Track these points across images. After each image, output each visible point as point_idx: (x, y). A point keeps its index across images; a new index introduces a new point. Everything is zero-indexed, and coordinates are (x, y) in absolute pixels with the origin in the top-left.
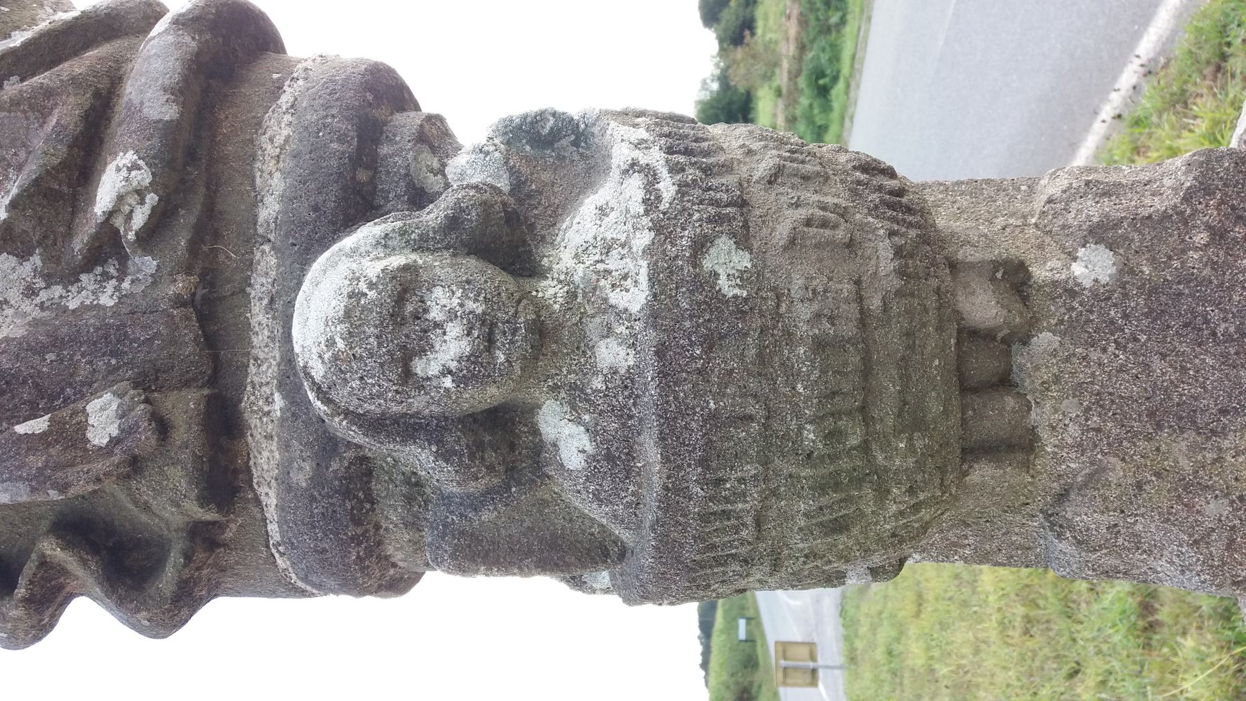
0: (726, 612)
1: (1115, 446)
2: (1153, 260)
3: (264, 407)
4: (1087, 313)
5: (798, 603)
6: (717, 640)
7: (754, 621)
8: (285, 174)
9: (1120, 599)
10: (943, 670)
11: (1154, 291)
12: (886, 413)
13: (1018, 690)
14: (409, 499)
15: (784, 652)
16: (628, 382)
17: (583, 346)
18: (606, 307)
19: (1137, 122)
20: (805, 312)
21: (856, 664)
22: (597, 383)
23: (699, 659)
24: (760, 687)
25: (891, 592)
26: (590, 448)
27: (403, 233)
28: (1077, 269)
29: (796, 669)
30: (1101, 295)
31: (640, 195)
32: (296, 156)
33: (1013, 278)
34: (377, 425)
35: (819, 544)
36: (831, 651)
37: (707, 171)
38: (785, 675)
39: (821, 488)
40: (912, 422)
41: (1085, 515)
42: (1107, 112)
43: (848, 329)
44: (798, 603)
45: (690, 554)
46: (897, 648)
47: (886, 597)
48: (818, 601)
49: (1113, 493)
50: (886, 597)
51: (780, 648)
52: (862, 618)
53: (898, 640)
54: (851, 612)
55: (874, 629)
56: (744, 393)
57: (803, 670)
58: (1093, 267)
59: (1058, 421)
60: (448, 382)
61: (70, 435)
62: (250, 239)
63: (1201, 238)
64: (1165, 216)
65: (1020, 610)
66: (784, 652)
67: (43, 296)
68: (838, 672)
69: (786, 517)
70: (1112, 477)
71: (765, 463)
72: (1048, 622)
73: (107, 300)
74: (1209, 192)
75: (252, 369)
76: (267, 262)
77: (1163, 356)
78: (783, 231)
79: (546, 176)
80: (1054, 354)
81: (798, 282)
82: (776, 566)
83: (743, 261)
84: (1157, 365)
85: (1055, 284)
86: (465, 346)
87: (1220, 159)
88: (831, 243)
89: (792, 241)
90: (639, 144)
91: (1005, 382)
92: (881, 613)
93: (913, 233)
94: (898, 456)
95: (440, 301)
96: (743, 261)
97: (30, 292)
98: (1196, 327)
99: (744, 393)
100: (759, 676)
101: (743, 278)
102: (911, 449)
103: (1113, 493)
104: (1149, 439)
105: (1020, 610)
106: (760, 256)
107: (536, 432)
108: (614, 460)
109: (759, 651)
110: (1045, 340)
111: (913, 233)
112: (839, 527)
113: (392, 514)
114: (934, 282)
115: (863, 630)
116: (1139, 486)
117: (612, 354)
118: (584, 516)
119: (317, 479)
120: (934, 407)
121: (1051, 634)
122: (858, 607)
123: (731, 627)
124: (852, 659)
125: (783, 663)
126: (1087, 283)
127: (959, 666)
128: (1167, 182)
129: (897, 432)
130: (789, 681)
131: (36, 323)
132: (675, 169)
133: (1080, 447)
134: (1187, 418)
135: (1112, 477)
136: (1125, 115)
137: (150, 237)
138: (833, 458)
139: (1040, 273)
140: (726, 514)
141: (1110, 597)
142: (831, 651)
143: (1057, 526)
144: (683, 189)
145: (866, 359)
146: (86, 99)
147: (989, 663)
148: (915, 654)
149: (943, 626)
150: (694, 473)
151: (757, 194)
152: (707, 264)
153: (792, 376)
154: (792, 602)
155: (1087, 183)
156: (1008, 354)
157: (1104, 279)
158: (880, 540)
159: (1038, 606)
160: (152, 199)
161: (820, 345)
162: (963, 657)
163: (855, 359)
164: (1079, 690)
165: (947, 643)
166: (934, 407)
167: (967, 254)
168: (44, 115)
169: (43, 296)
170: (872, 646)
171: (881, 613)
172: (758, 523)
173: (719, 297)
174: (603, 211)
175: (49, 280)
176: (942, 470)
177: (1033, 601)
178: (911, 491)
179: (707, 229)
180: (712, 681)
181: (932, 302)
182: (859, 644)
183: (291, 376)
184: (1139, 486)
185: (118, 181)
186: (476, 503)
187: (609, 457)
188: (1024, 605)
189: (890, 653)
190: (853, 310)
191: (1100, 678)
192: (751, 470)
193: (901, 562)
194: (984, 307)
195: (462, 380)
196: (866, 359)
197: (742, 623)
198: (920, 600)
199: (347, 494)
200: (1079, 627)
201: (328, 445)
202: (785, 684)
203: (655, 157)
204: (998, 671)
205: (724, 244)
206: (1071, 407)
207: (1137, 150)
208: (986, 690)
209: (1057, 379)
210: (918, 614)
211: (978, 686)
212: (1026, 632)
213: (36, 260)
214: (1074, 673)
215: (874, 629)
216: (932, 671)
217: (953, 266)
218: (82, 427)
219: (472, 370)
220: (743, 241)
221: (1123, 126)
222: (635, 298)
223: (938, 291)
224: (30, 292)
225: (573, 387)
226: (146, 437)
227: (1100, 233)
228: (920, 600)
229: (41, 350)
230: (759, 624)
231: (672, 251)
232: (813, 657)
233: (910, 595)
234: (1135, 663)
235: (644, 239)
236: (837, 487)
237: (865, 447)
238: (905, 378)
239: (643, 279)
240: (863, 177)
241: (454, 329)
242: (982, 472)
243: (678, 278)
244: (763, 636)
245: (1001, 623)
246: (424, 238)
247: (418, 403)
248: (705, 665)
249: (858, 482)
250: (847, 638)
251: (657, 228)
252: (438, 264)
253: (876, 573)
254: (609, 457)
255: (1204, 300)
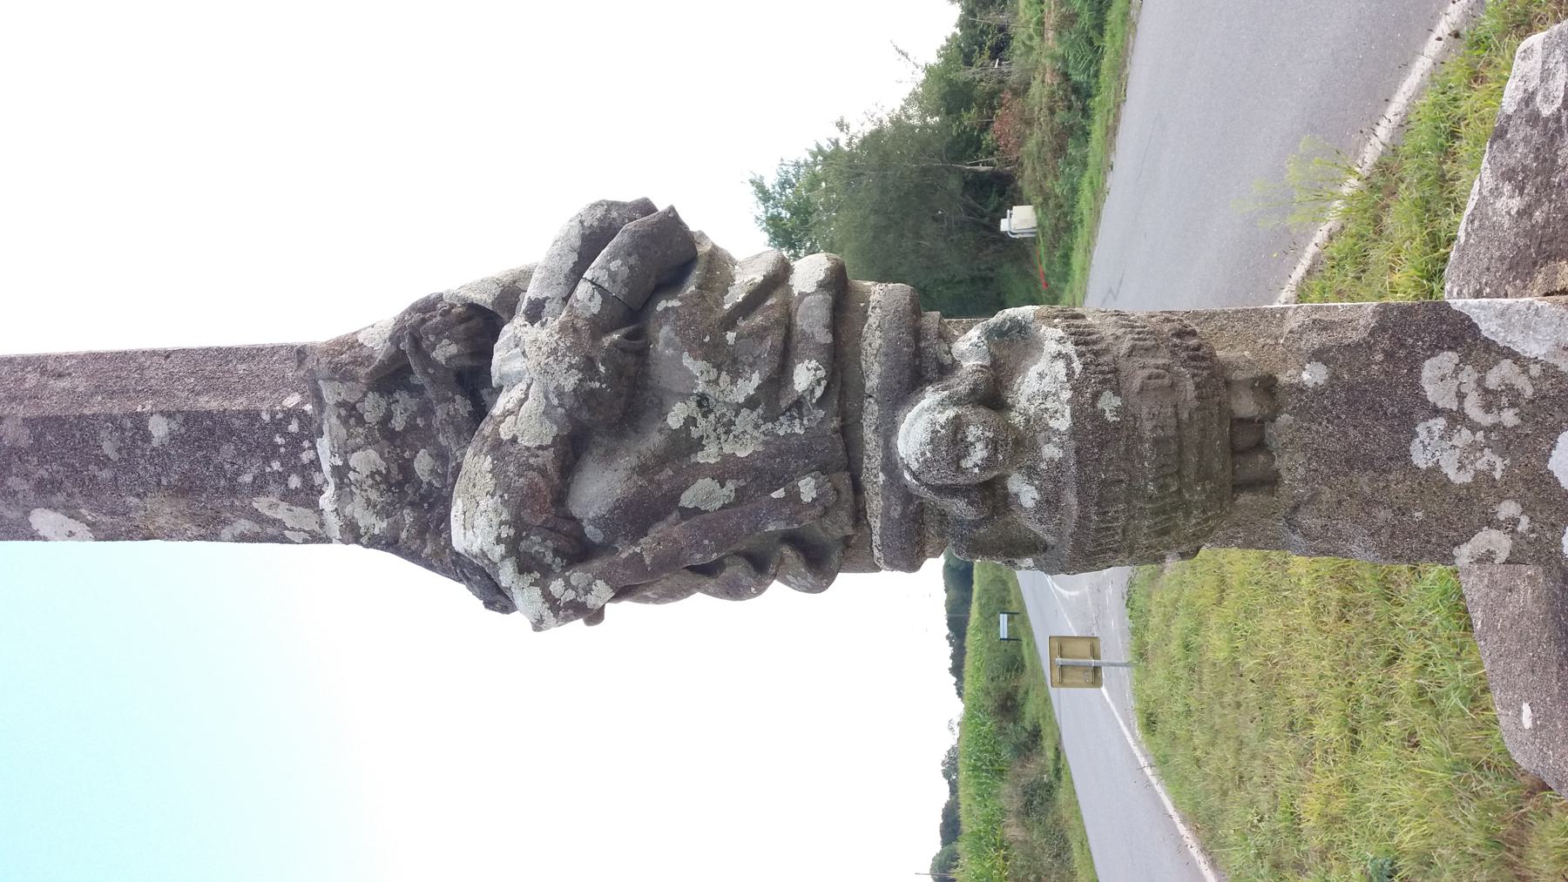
0: (982, 606)
1: (1326, 480)
2: (1350, 371)
3: (875, 479)
4: (1310, 403)
5: (1074, 593)
6: (972, 639)
7: (1018, 616)
8: (881, 364)
9: (1441, 579)
10: (1248, 663)
11: (1351, 389)
12: (1190, 472)
13: (1332, 681)
14: (941, 522)
15: (1061, 648)
16: (1059, 465)
17: (1035, 447)
18: (1047, 428)
19: (1477, 43)
20: (1148, 425)
21: (1146, 660)
22: (1043, 466)
23: (949, 663)
24: (1027, 693)
25: (1188, 576)
26: (1037, 497)
27: (950, 397)
28: (1305, 376)
29: (1074, 667)
30: (1318, 392)
31: (1064, 371)
32: (886, 355)
33: (1267, 386)
34: (940, 490)
35: (1154, 541)
36: (1116, 646)
37: (1097, 354)
38: (1062, 674)
39: (1155, 513)
40: (1205, 475)
41: (1308, 520)
42: (1443, 28)
43: (1171, 432)
44: (1074, 593)
45: (1089, 547)
46: (1195, 640)
47: (1182, 583)
48: (1098, 590)
49: (1324, 507)
50: (1182, 583)
51: (1056, 644)
52: (1154, 609)
53: (1196, 632)
54: (1140, 601)
55: (1168, 620)
56: (1119, 469)
57: (1085, 668)
58: (1313, 375)
59: (1292, 467)
60: (976, 470)
61: (793, 496)
62: (861, 395)
63: (1379, 357)
64: (1358, 345)
65: (1336, 594)
66: (1061, 648)
67: (763, 428)
68: (1123, 671)
69: (1137, 528)
70: (1324, 498)
71: (1128, 503)
72: (1366, 605)
73: (799, 430)
74: (1385, 330)
75: (866, 460)
76: (872, 412)
77: (1355, 427)
78: (1136, 383)
79: (1005, 352)
80: (1290, 427)
81: (1145, 410)
82: (1131, 553)
83: (1117, 402)
84: (1352, 432)
85: (1291, 385)
86: (985, 454)
87: (1391, 310)
88: (1161, 388)
89: (1142, 389)
90: (1060, 340)
91: (1260, 446)
92: (1177, 600)
93: (1205, 373)
94: (1197, 495)
95: (973, 432)
96: (1117, 402)
97: (757, 426)
98: (1375, 410)
99: (1119, 469)
100: (1026, 680)
101: (1118, 411)
102: (1204, 490)
103: (1324, 507)
104: (1346, 475)
105: (1336, 594)
106: (1125, 399)
107: (1005, 488)
108: (1050, 502)
109: (1026, 652)
110: (1285, 418)
111: (1205, 373)
112: (1165, 532)
113: (932, 530)
114: (1217, 399)
115: (1154, 621)
116: (1339, 502)
117: (1051, 451)
118: (1027, 529)
119: (903, 515)
120: (1217, 466)
121: (1370, 618)
122: (1149, 596)
123: (990, 621)
124: (1142, 655)
125: (1059, 660)
126: (1311, 385)
127: (1268, 659)
128: (1362, 322)
129: (1196, 482)
130: (1066, 681)
131: (765, 443)
132: (1081, 355)
133: (1305, 480)
134: (1368, 463)
135: (1324, 498)
136: (1464, 31)
137: (821, 402)
138: (1163, 498)
139: (1283, 378)
140: (1108, 529)
141: (1431, 576)
142: (1116, 646)
143: (1293, 526)
144: (1086, 366)
145: (1180, 446)
146: (782, 331)
147: (1301, 652)
148: (1217, 646)
149: (1249, 614)
150: (1094, 509)
151: (1123, 363)
152: (1099, 406)
153: (1142, 458)
154: (1066, 593)
155: (1314, 321)
156: (1262, 428)
157: (1321, 382)
158: (1186, 538)
159: (1355, 589)
160: (824, 383)
161: (1156, 442)
162: (1271, 648)
163: (1174, 447)
164: (1396, 677)
165: (1253, 633)
166: (1217, 466)
167: (1239, 375)
168: (763, 338)
169: (763, 428)
170: (1166, 640)
171: (1177, 600)
172: (1124, 532)
173: (1107, 423)
174: (1041, 376)
175: (765, 420)
176: (1221, 499)
177: (1350, 583)
178: (1204, 512)
179: (1099, 387)
180: (967, 687)
181: (1216, 410)
182: (1150, 638)
183: (891, 465)
184: (1339, 502)
185: (805, 376)
186: (977, 524)
187: (1048, 501)
188: (1340, 588)
189: (1187, 647)
190: (1173, 422)
191: (1419, 664)
192: (1121, 506)
193: (1198, 549)
194: (1246, 406)
195: (982, 469)
196: (1180, 446)
197: (1003, 618)
198: (1222, 586)
199: (915, 521)
200: (1398, 610)
201: (908, 496)
202: (1062, 684)
203: (1069, 348)
204: (1310, 661)
205: (1108, 394)
206: (1300, 458)
207: (1476, 77)
208: (1297, 682)
209: (1292, 442)
210: (1219, 602)
211: (1288, 679)
212: (1342, 617)
213: (760, 411)
214: (1391, 661)
215: (1168, 620)
216: (1236, 664)
217: (1228, 384)
218: (798, 493)
219: (988, 464)
220: (1117, 392)
221: (1462, 45)
222: (1063, 423)
223: (1219, 404)
224: (757, 426)
225: (1029, 467)
226: (832, 498)
227: (1319, 355)
228: (1222, 586)
229: (773, 457)
230: (1025, 620)
231: (1082, 400)
232: (1094, 654)
233: (1211, 580)
234: (1455, 645)
235: (1066, 395)
236: (1164, 512)
237: (1179, 491)
238: (1201, 453)
239: (1068, 413)
240: (1178, 341)
241: (979, 446)
242: (1245, 498)
243: (1086, 415)
244: (1030, 634)
245: (1315, 608)
246: (959, 399)
247: (961, 480)
248: (957, 670)
249: (1175, 509)
250: (1134, 632)
251: (1074, 389)
252: (967, 412)
253: (1183, 556)
254: (1048, 501)
255: (1380, 394)
